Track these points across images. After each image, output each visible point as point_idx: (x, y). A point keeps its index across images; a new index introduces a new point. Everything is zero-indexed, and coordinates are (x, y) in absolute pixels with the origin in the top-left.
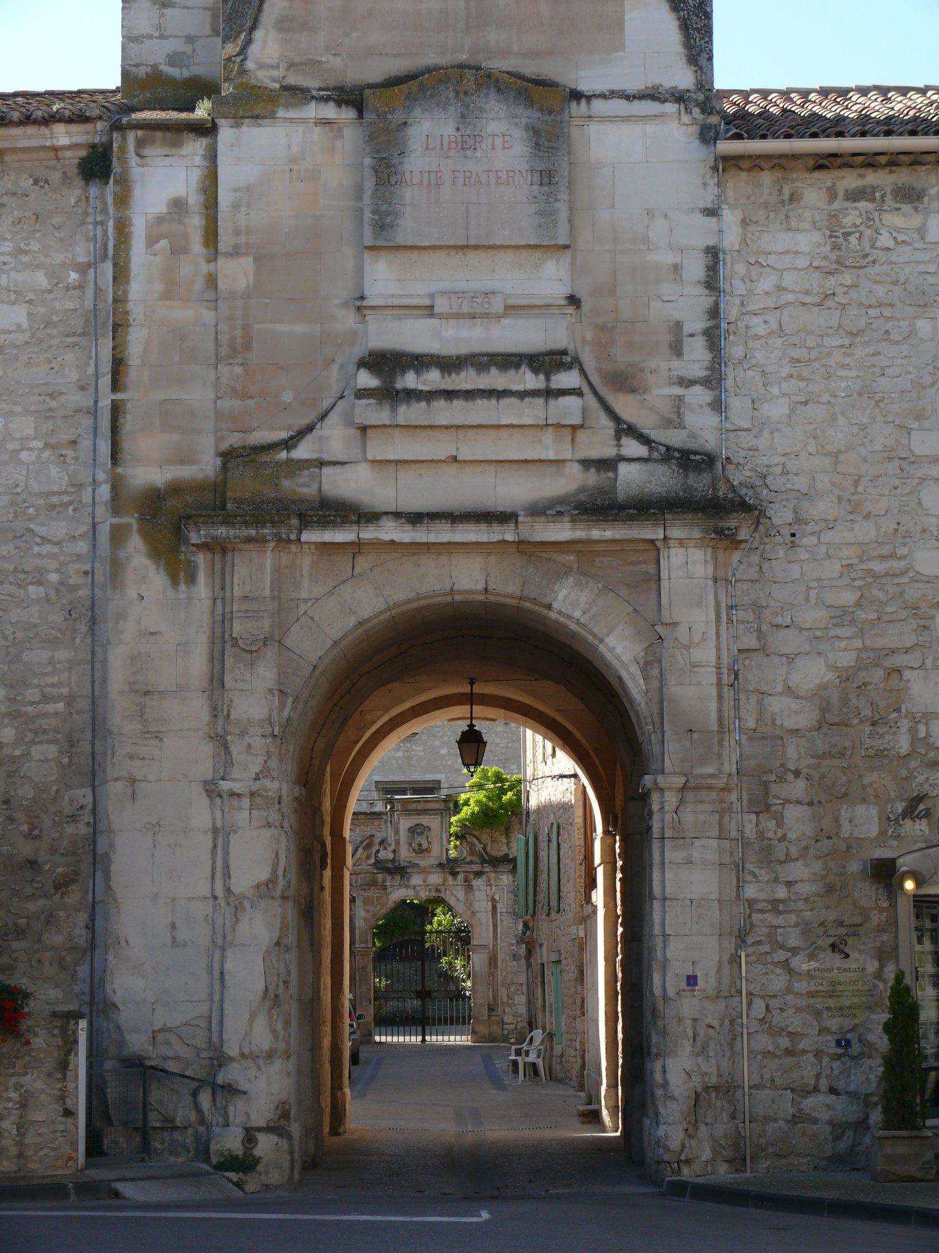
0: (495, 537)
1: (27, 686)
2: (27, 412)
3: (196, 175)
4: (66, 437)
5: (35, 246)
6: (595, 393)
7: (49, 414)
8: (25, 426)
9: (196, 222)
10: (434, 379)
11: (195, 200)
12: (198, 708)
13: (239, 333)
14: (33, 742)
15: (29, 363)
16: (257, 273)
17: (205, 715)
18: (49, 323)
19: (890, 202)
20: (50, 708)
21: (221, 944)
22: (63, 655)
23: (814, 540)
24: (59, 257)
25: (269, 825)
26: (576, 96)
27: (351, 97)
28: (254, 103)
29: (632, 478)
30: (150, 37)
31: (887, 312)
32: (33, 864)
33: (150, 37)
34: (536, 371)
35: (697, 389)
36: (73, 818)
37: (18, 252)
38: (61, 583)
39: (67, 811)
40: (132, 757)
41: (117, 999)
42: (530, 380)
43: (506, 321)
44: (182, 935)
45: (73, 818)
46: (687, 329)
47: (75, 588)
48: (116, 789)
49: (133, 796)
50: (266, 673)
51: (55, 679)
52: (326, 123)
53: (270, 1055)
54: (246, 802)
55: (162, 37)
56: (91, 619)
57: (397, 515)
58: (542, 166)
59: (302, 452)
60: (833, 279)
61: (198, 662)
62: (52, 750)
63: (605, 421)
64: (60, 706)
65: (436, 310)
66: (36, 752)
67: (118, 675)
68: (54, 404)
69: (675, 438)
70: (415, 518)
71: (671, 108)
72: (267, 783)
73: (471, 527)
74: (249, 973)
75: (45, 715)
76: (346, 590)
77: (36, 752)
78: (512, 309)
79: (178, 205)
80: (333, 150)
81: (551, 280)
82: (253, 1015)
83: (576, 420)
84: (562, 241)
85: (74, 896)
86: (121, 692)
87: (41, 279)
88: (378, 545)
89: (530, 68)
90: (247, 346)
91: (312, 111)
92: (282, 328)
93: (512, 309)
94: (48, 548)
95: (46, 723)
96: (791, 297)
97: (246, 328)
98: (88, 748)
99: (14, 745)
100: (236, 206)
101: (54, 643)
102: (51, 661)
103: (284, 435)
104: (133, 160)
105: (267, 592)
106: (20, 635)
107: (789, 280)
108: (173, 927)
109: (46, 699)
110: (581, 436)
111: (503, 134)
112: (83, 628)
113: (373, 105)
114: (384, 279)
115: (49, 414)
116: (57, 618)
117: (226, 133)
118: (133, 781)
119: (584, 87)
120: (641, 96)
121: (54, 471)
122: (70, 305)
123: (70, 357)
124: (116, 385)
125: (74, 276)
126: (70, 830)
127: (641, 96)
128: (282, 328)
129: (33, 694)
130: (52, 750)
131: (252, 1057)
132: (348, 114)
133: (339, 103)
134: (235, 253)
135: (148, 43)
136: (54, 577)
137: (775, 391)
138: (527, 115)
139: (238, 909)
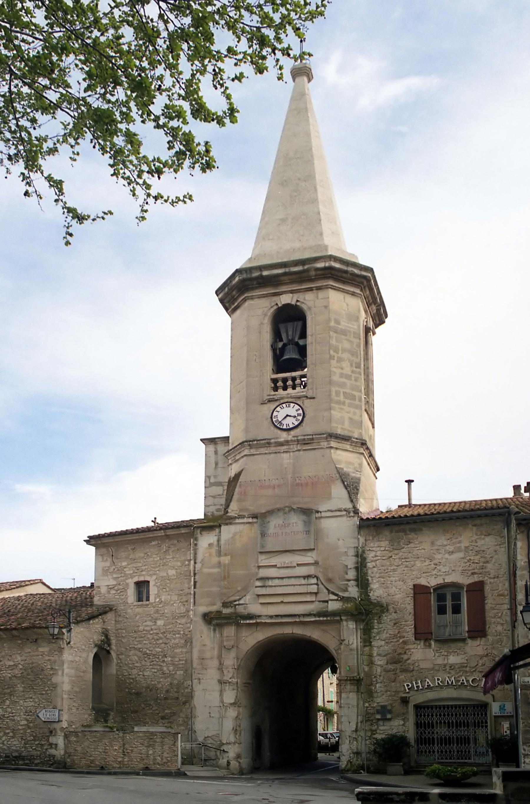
0: (293, 620)
1: (176, 657)
2: (176, 594)
3: (216, 538)
4: (185, 600)
5: (178, 556)
6: (323, 584)
7: (180, 595)
8: (175, 598)
9: (215, 548)
10: (277, 582)
11: (216, 543)
12: (216, 662)
13: (226, 574)
14: (177, 670)
15: (176, 583)
16: (231, 560)
17: (218, 664)
18: (181, 574)
19: (408, 532)
20: (181, 662)
21: (222, 718)
22: (184, 650)
23: (386, 618)
24: (183, 558)
25: (234, 690)
26: (318, 512)
27: (255, 516)
28: (229, 521)
29: (334, 606)
30: (211, 505)
31: (407, 560)
32: (177, 698)
33: (211, 505)
34: (304, 579)
35: (352, 582)
36: (187, 688)
37: (173, 558)
38: (184, 634)
39: (186, 686)
40: (199, 674)
41: (196, 729)
42: (303, 582)
43: (297, 568)
44: (212, 715)
45: (187, 688)
46: (349, 567)
47: (187, 635)
48: (195, 682)
49: (200, 683)
50: (233, 654)
51: (182, 656)
52: (249, 523)
53: (234, 743)
54: (228, 684)
55: (215, 505)
56: (188, 641)
57: (266, 616)
58: (307, 530)
59: (241, 602)
60: (392, 553)
61: (216, 652)
62: (182, 672)
63: (325, 591)
64: (184, 662)
65: (278, 566)
66: (178, 673)
67: (195, 656)
68: (182, 592)
69: (346, 595)
70: (271, 617)
71: (345, 513)
72: (233, 680)
73: (290, 618)
74: (229, 724)
75: (180, 664)
76: (255, 633)
77: (178, 673)
78: (298, 565)
79: (210, 545)
80: (251, 530)
81: (309, 558)
82: (230, 734)
83: (316, 591)
84: (312, 548)
85: (187, 705)
86: (197, 659)
87: (179, 564)
88: (261, 623)
89: (305, 506)
90: (228, 577)
91: (245, 520)
92: (238, 572)
93: (298, 565)
94: (181, 626)
95: (181, 666)
96: (379, 558)
97: (228, 573)
98: (189, 673)
99: (173, 671)
100: (225, 544)
101: (182, 647)
102: (181, 652)
103: (238, 597)
104: (199, 535)
105: (233, 635)
106: (174, 646)
107: (378, 553)
108: (210, 713)
109: (180, 660)
110: (319, 595)
111: (296, 522)
112: (189, 644)
113: (260, 517)
114: (263, 560)
115: (180, 595)
116: (183, 641)
117: (223, 527)
118: (199, 679)
119: (320, 510)
120: (336, 511)
121: (182, 607)
122: (186, 569)
123: (186, 581)
124: (195, 588)
125: (187, 562)
126: (186, 690)
127: (336, 511)
128: (238, 572)
129: (177, 659)
130: (182, 672)
131: (229, 744)
132: (255, 520)
133: (253, 518)
134: (226, 555)
135: (211, 507)
136: (182, 632)
137: (375, 581)
138: (304, 517)
139: (226, 710)
